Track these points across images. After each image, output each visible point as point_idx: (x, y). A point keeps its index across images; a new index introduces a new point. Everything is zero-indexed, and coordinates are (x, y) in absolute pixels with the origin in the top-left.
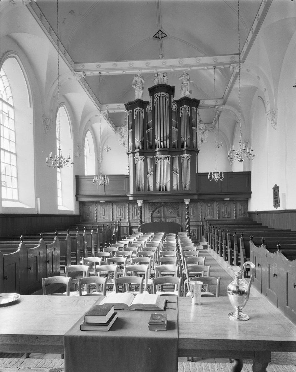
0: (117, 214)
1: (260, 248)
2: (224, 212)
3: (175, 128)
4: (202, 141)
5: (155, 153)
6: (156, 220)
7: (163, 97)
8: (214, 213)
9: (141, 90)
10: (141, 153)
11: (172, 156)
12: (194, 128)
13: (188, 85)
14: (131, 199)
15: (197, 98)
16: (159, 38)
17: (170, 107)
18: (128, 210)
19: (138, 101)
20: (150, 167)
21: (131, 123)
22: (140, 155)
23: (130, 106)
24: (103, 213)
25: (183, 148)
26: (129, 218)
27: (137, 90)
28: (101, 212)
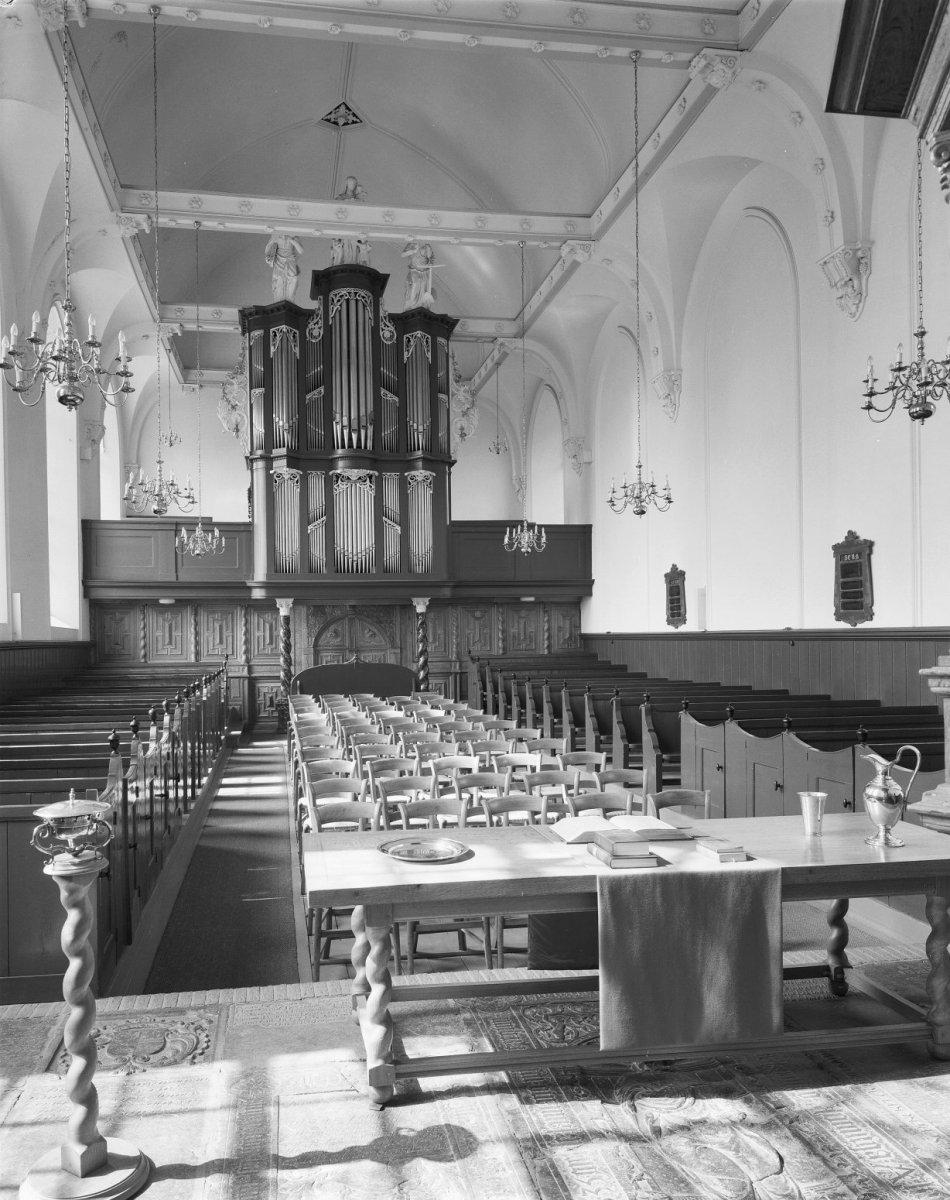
0: (211, 639)
1: (719, 729)
2: (519, 634)
3: (390, 395)
4: (463, 435)
5: (331, 464)
6: (328, 659)
7: (357, 300)
8: (490, 637)
9: (292, 274)
10: (293, 461)
11: (380, 474)
12: (442, 396)
13: (427, 275)
14: (258, 594)
15: (451, 313)
16: (336, 123)
17: (375, 330)
18: (244, 628)
19: (284, 307)
20: (317, 500)
21: (260, 368)
22: (289, 466)
23: (256, 318)
24: (167, 635)
25: (408, 453)
26: (247, 652)
27: (280, 273)
28: (159, 633)
